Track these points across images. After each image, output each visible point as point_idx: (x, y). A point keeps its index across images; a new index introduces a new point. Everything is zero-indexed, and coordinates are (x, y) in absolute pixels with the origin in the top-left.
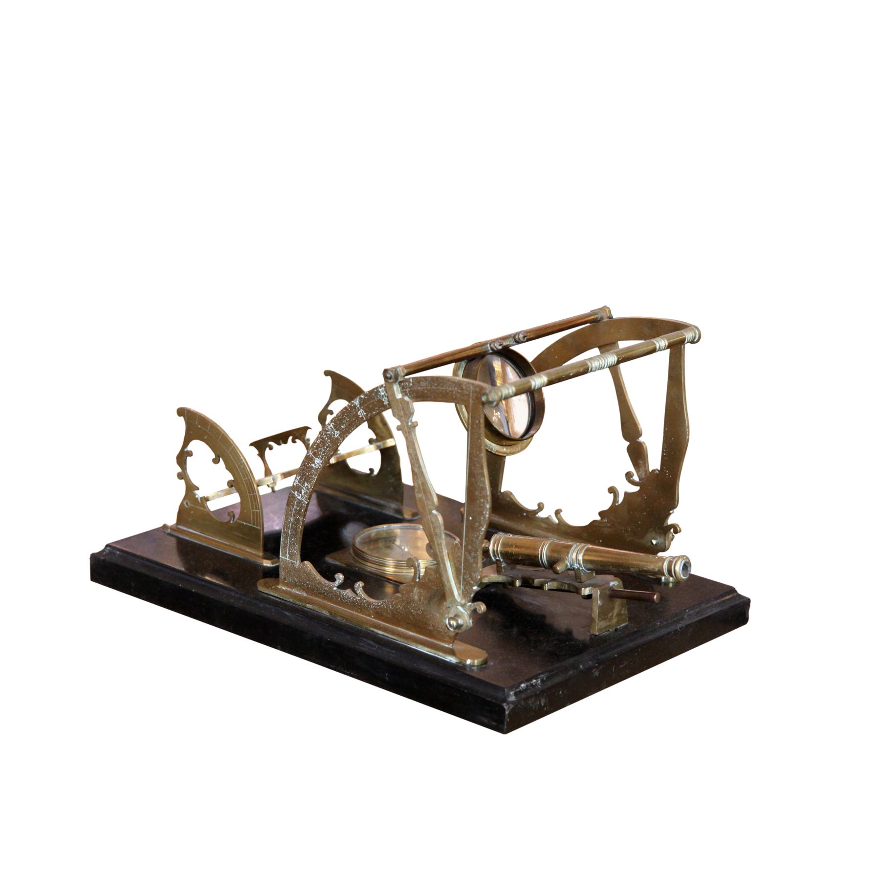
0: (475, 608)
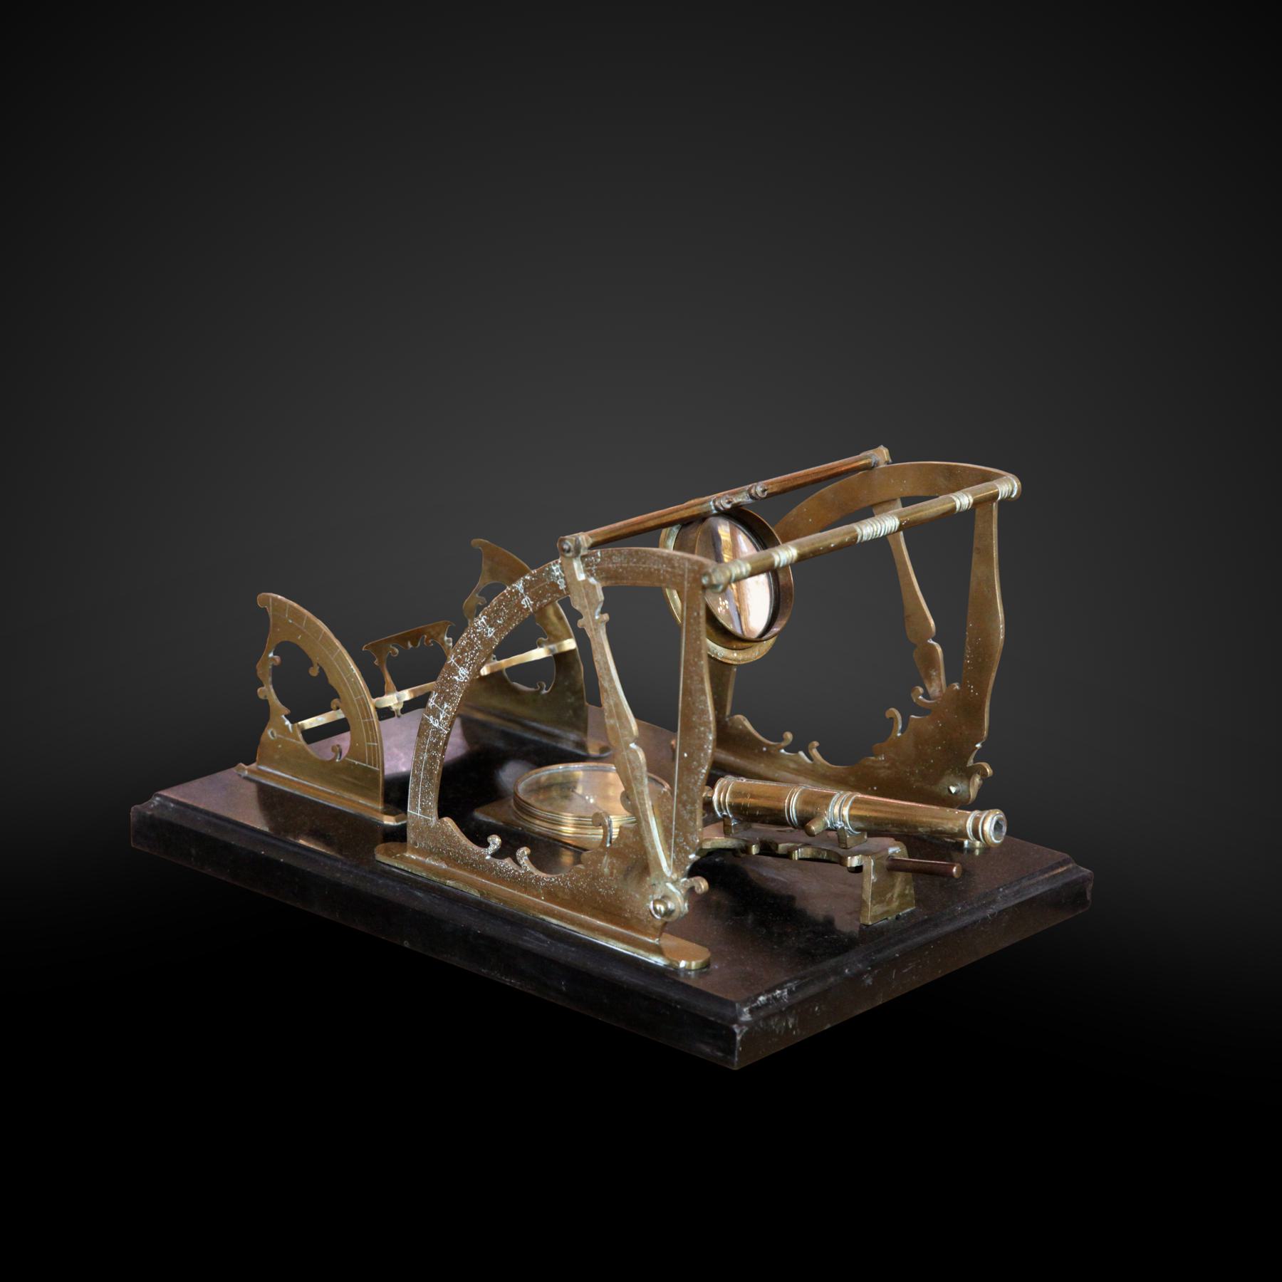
0: (692, 885)
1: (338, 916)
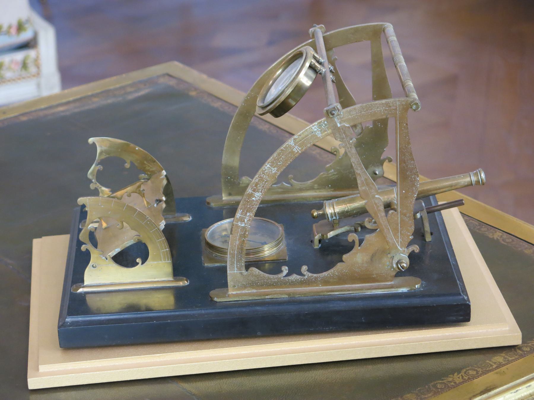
0: (412, 250)
1: (211, 335)
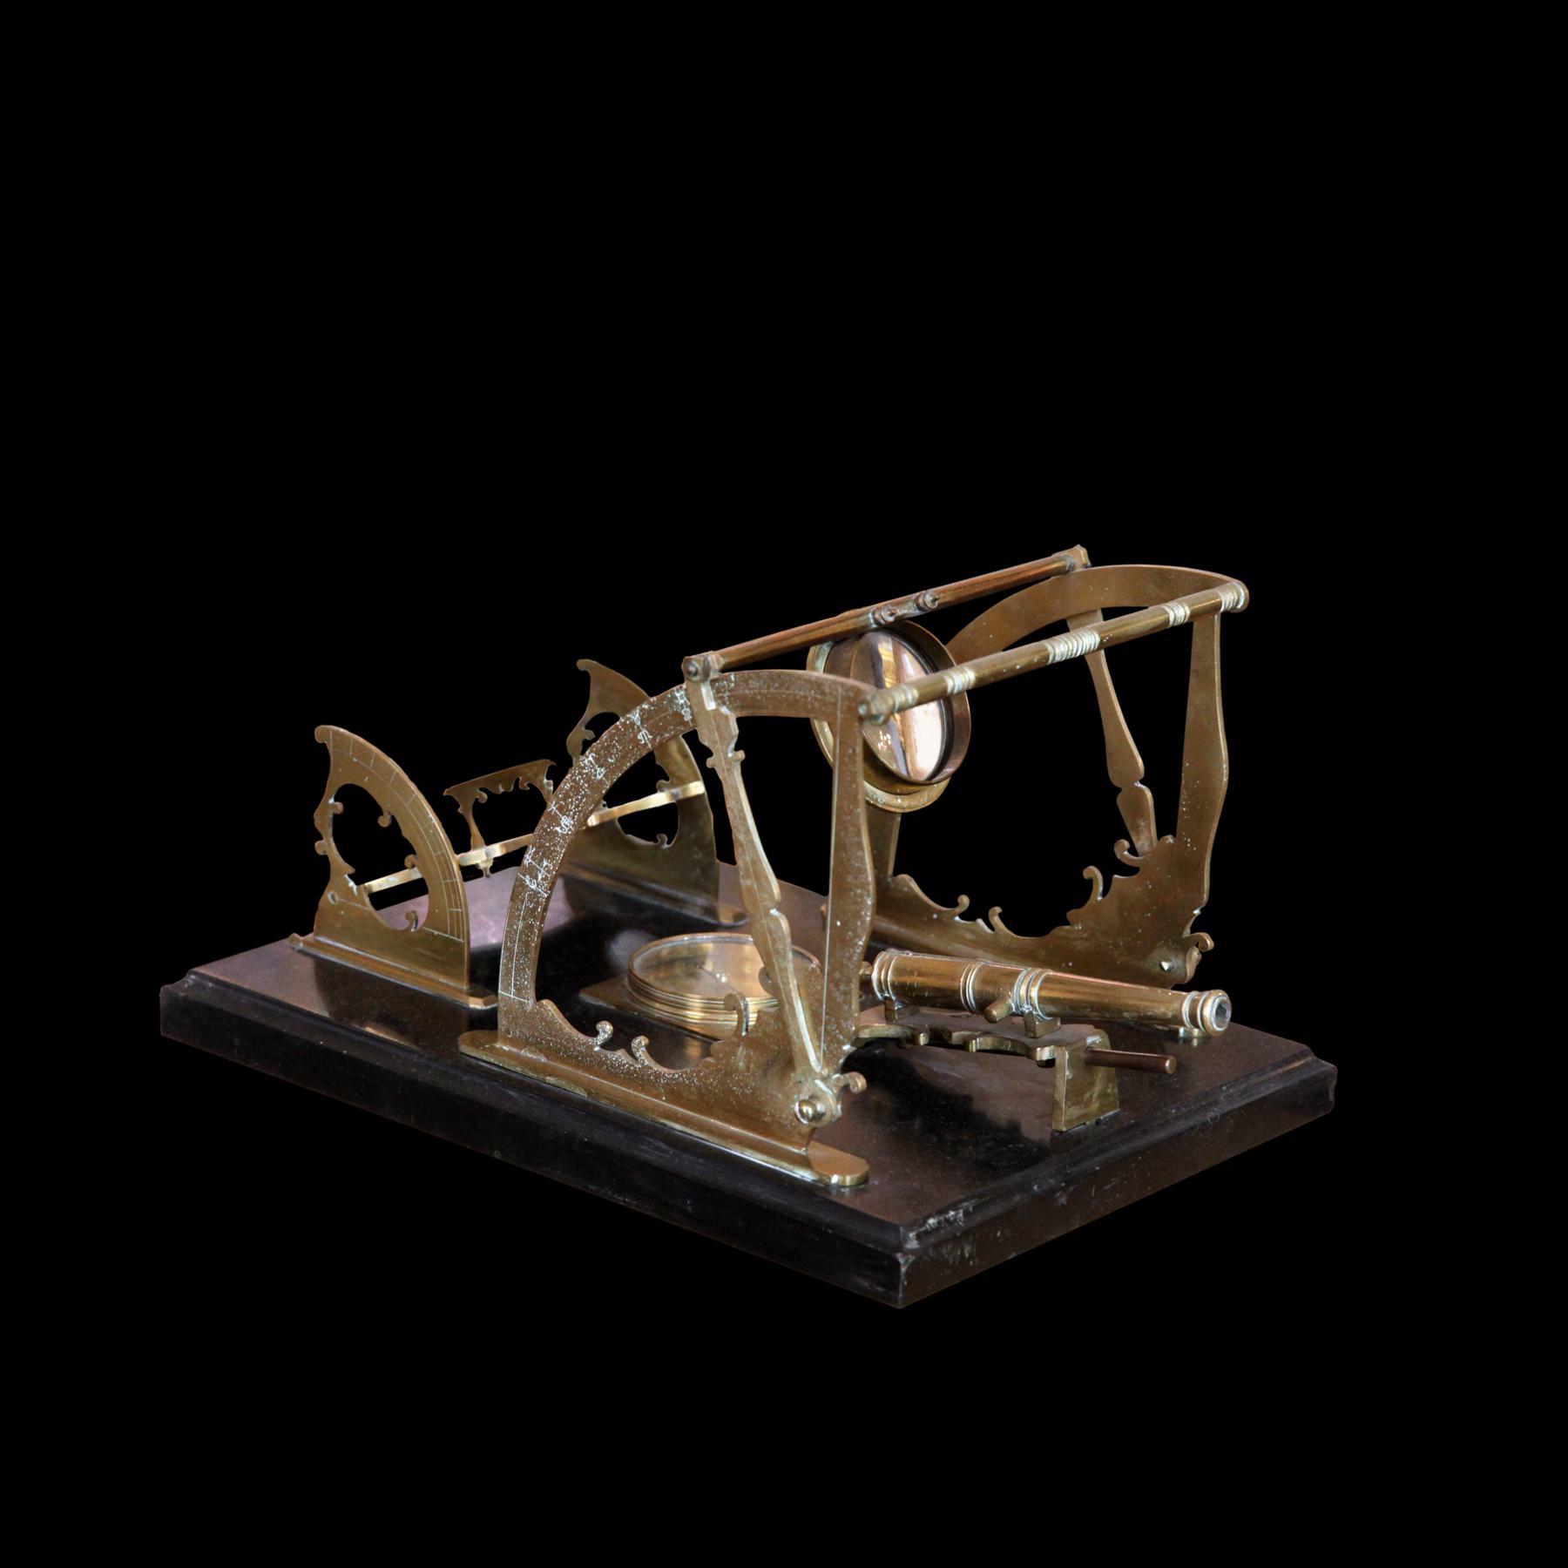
0: (846, 1083)
1: (413, 1120)
